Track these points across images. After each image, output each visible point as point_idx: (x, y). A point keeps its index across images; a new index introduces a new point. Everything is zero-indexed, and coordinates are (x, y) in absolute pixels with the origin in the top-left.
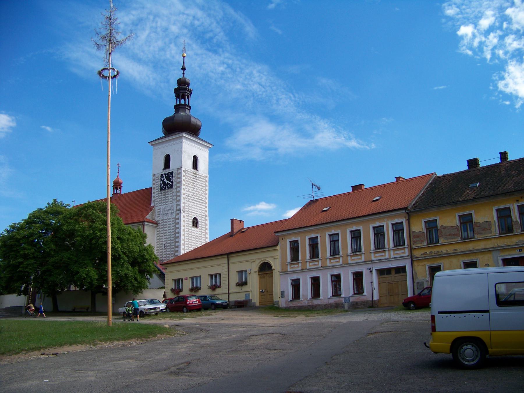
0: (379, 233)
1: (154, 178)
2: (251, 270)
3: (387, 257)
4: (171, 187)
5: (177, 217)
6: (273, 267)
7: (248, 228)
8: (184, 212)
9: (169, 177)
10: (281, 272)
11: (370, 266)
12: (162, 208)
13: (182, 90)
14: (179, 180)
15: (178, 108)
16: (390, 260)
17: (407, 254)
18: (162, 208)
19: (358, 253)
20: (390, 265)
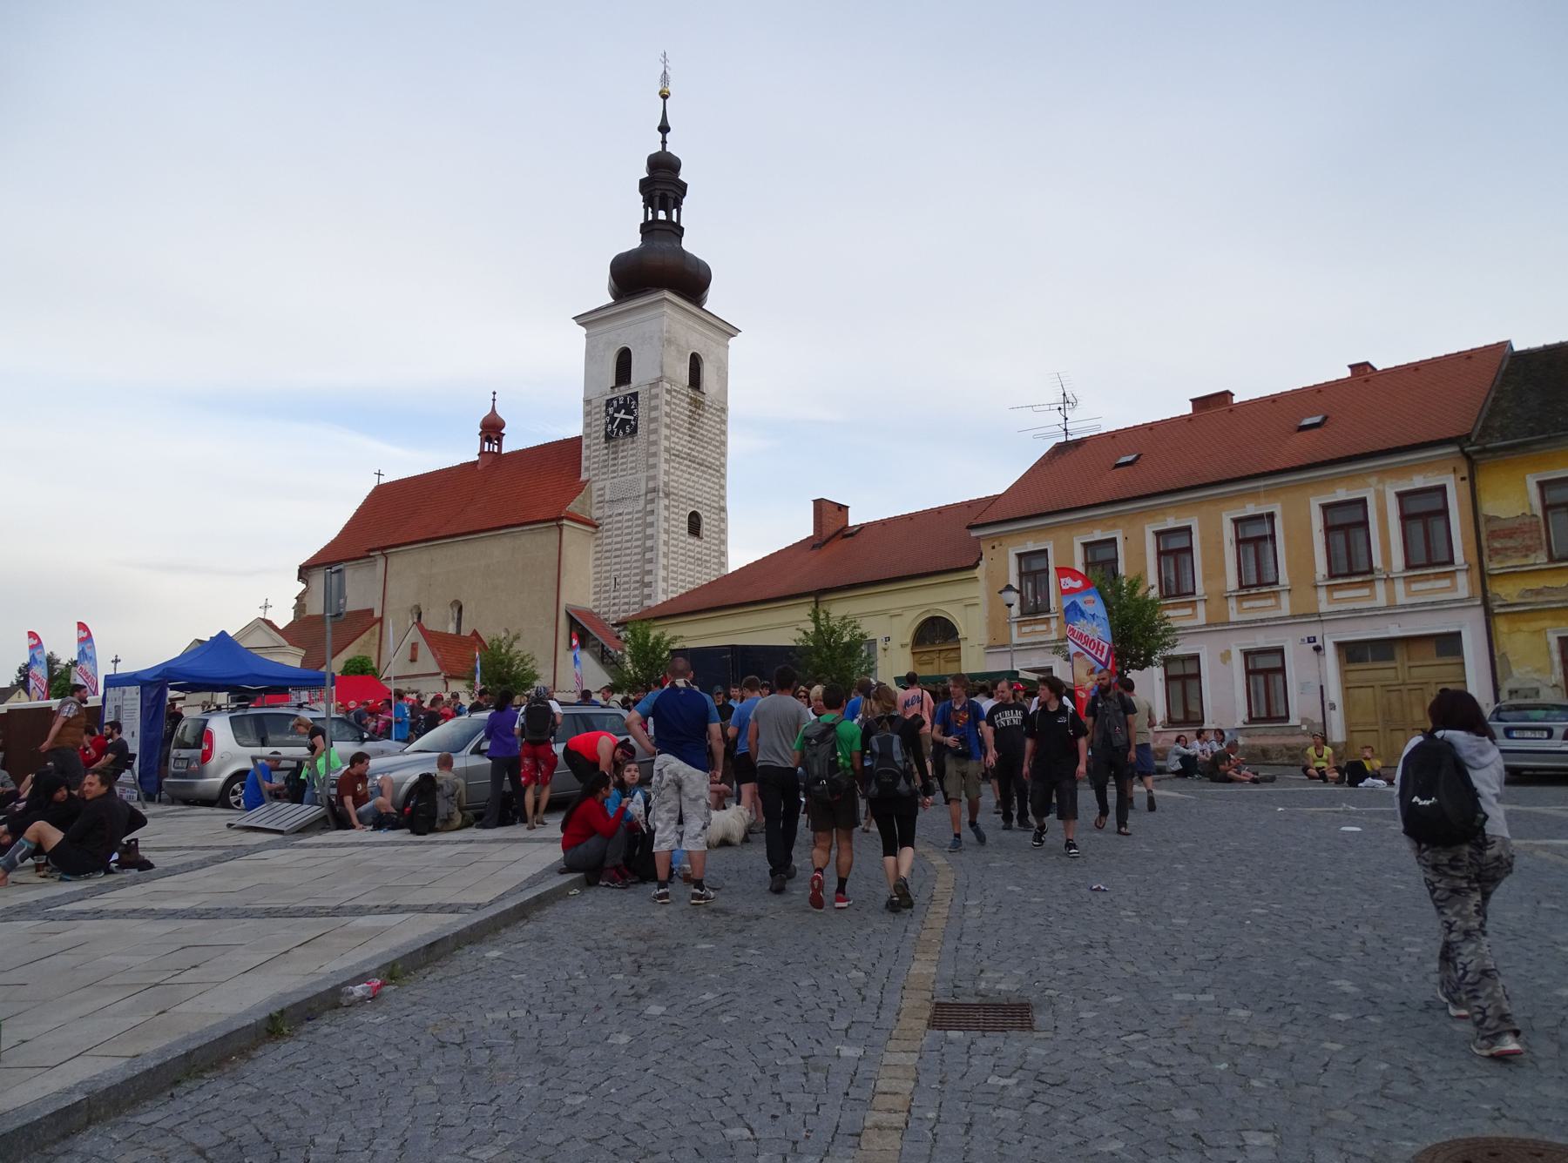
0: (1347, 524)
3: (1381, 600)
4: (634, 430)
5: (649, 508)
7: (862, 527)
8: (667, 495)
9: (629, 404)
10: (990, 647)
11: (1314, 631)
13: (663, 183)
14: (653, 414)
15: (647, 229)
16: (1392, 610)
17: (1463, 592)
19: (1265, 590)
20: (1394, 630)
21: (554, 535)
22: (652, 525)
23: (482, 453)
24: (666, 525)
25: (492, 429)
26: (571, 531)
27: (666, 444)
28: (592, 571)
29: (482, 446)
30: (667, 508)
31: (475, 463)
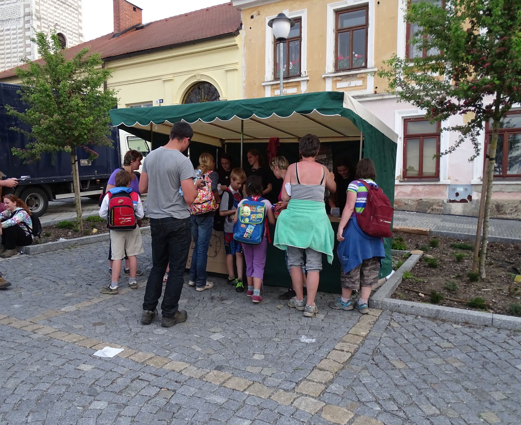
5: (27, 26)
8: (39, 19)
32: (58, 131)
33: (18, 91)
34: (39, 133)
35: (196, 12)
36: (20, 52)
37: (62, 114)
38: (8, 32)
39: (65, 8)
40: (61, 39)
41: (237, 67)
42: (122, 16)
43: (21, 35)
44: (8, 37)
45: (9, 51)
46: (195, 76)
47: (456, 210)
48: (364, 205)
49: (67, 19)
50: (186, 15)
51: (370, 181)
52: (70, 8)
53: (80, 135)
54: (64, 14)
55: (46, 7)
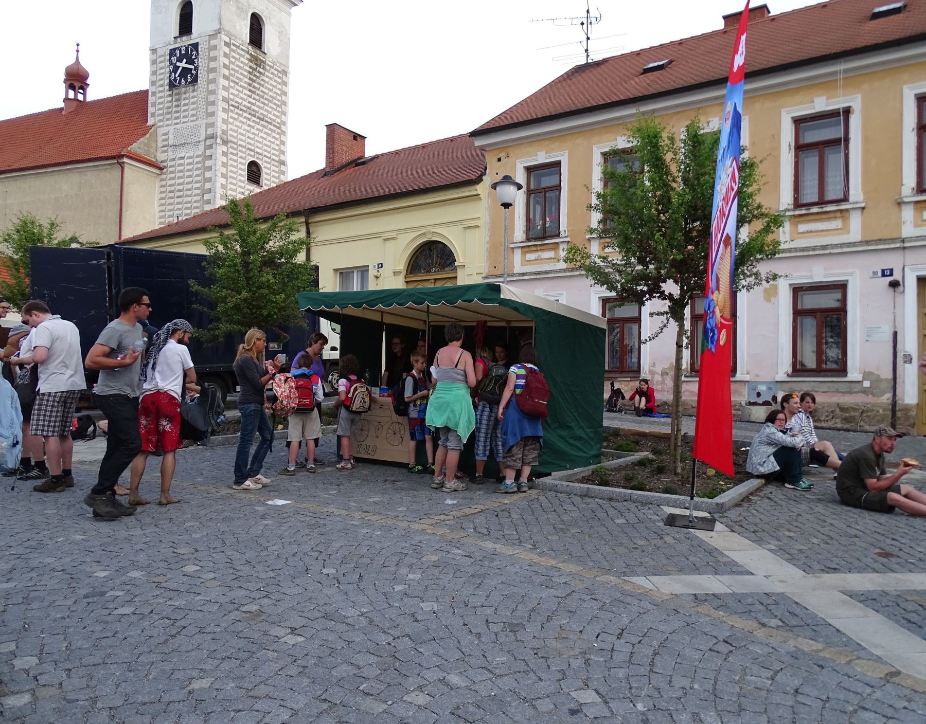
1: (154, 57)
2: (381, 266)
4: (195, 80)
5: (208, 152)
6: (460, 260)
7: (374, 158)
8: (225, 142)
9: (190, 54)
11: (892, 261)
12: (172, 132)
14: (212, 65)
18: (172, 132)
21: (116, 173)
22: (210, 169)
23: (66, 100)
24: (224, 170)
25: (76, 78)
26: (132, 170)
27: (225, 94)
28: (157, 209)
29: (67, 93)
30: (225, 154)
31: (61, 109)
32: (246, 310)
33: (204, 263)
34: (225, 313)
35: (438, 142)
36: (196, 189)
37: (250, 290)
38: (182, 161)
39: (262, 126)
40: (254, 168)
41: (478, 223)
42: (337, 147)
43: (200, 165)
44: (182, 168)
45: (181, 187)
46: (424, 234)
47: (757, 415)
48: (522, 387)
49: (265, 142)
50: (424, 146)
51: (530, 365)
52: (270, 126)
53: (269, 315)
54: (261, 134)
55: (236, 126)
